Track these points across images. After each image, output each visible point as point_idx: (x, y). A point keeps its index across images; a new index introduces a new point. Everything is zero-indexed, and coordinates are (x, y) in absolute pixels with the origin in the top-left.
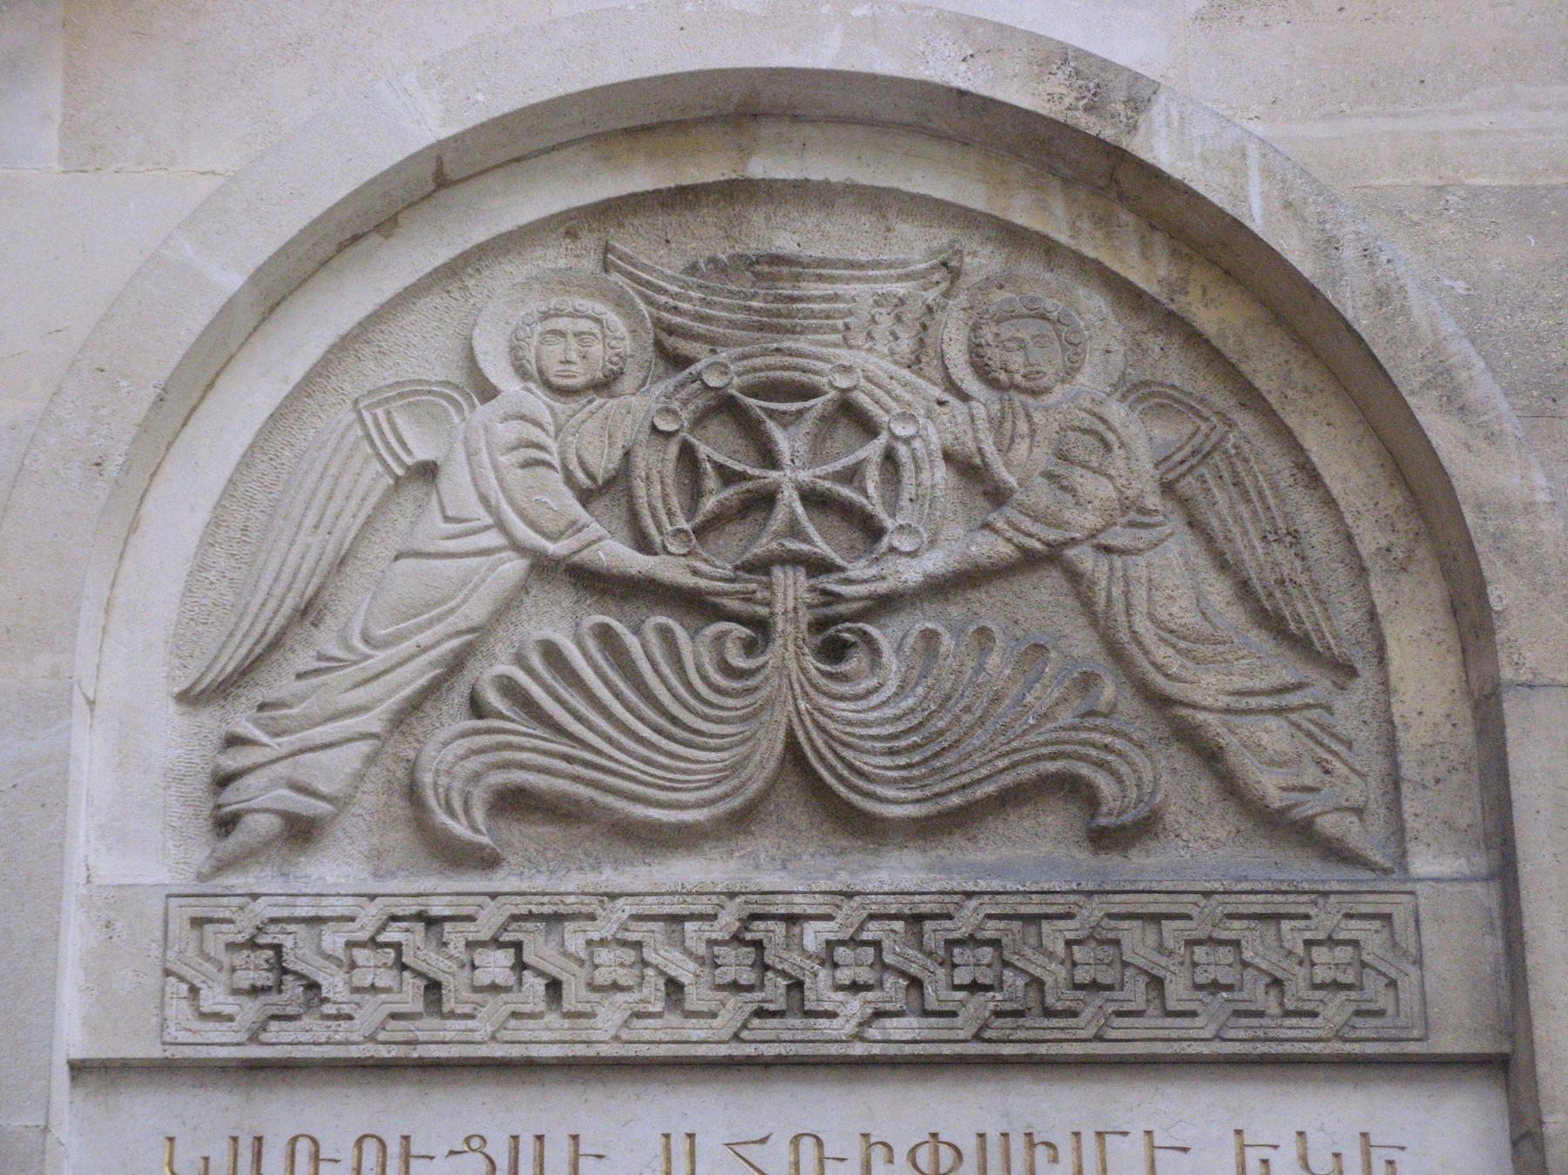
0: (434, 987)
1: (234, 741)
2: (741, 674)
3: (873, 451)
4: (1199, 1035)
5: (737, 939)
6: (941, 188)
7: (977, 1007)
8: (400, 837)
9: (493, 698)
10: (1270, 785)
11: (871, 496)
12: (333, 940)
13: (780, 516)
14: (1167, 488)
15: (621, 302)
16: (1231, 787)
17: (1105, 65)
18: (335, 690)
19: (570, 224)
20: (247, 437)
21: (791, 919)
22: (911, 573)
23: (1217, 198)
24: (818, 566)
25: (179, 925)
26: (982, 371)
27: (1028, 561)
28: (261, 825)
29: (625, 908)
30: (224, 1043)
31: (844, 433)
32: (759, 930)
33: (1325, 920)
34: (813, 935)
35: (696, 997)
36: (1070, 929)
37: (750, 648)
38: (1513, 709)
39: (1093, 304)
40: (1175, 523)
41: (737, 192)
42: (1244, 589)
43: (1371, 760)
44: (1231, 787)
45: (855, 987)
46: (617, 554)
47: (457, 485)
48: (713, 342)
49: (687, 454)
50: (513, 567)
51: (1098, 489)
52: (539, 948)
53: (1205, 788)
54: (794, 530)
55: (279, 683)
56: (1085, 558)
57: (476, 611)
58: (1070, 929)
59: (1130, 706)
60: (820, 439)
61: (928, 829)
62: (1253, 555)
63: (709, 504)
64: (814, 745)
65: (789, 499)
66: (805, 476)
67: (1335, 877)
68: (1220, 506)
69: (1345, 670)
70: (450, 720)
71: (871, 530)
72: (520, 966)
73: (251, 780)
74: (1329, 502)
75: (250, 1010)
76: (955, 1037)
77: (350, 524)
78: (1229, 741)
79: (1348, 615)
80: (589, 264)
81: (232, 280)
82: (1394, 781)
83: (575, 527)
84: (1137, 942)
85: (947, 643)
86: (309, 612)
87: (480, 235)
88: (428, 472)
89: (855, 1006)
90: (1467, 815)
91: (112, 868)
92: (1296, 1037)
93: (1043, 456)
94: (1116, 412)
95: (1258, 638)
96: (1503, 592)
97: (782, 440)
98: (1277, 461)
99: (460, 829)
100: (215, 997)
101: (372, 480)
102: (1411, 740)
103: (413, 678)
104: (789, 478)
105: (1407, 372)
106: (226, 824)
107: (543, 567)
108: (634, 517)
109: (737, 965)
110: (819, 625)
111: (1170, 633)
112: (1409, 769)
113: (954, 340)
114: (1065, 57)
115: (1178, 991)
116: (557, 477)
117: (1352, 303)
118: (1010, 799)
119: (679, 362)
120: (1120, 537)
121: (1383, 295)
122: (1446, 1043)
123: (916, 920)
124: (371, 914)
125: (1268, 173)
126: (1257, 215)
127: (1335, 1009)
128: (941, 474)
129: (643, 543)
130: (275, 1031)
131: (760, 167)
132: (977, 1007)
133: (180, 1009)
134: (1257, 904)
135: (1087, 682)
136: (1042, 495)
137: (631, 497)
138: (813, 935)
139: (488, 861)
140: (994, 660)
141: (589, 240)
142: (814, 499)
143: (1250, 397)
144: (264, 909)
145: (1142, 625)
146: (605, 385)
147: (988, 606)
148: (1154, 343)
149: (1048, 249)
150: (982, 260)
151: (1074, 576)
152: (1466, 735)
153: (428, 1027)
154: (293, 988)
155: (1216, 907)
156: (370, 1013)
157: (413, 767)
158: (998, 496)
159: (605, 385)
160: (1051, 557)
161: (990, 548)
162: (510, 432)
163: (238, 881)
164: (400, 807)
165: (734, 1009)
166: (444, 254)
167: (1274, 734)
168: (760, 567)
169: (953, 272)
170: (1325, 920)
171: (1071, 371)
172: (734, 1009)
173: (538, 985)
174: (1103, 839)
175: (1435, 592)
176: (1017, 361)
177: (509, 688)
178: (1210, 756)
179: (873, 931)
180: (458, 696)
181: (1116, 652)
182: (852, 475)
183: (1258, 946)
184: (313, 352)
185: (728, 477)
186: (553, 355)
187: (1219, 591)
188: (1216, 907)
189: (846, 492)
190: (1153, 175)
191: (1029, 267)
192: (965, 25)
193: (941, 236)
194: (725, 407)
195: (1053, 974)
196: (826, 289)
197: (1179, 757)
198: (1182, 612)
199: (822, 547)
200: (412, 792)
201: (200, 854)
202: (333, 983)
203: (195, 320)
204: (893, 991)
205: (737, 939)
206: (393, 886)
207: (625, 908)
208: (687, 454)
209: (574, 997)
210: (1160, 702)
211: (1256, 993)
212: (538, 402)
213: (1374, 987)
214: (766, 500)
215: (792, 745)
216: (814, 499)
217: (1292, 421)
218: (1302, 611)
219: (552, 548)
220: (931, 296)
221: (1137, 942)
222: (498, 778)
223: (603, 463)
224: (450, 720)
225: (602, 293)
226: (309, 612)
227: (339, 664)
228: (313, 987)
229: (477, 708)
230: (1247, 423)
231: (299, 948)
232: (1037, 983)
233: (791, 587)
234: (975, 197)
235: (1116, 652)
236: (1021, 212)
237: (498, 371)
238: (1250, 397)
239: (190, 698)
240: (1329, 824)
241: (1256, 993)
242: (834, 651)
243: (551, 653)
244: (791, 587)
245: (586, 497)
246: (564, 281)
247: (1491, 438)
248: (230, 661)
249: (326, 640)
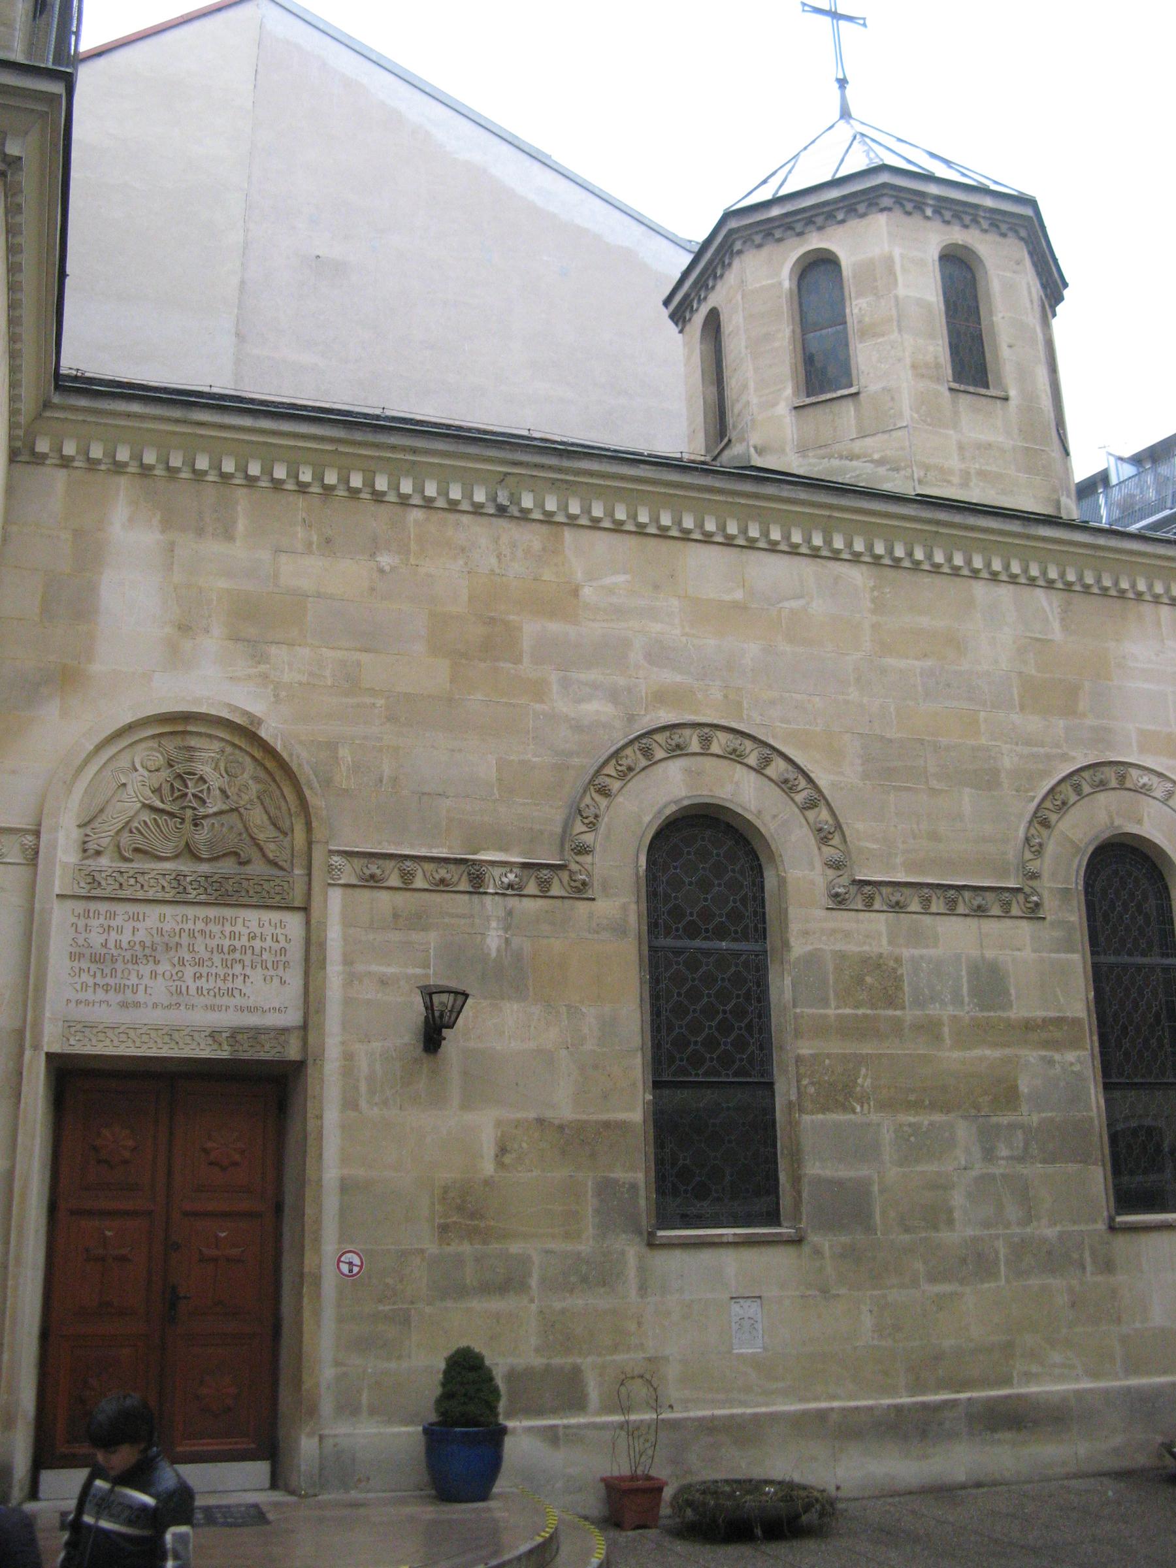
0: (121, 884)
1: (87, 835)
2: (177, 828)
3: (205, 787)
4: (254, 901)
5: (175, 879)
6: (222, 735)
7: (216, 894)
8: (116, 855)
9: (134, 831)
10: (271, 855)
11: (204, 796)
12: (104, 875)
13: (188, 799)
14: (259, 797)
15: (162, 754)
16: (264, 855)
17: (255, 716)
18: (105, 827)
19: (153, 737)
20: (92, 776)
21: (185, 876)
22: (211, 811)
23: (272, 744)
24: (194, 809)
25: (76, 871)
26: (226, 772)
27: (232, 810)
28: (91, 852)
29: (156, 872)
30: (83, 892)
31: (201, 783)
32: (179, 878)
33: (278, 881)
34: (189, 879)
35: (168, 889)
36: (233, 881)
37: (181, 823)
38: (314, 846)
39: (248, 760)
40: (259, 804)
41: (185, 733)
42: (270, 818)
43: (288, 852)
44: (264, 855)
45: (195, 889)
46: (158, 804)
47: (130, 789)
48: (178, 763)
49: (172, 786)
50: (139, 805)
51: (246, 797)
52: (140, 879)
53: (259, 855)
54: (190, 802)
55: (96, 824)
56: (242, 810)
57: (132, 813)
58: (233, 881)
59: (248, 838)
60: (197, 783)
61: (209, 860)
62: (273, 811)
63: (175, 795)
64: (191, 842)
65: (190, 795)
66: (193, 791)
67: (281, 873)
68: (267, 801)
69: (286, 834)
70: (126, 834)
71: (204, 802)
72: (137, 882)
73: (91, 843)
74: (286, 802)
75: (88, 887)
76: (211, 899)
77: (110, 794)
78: (264, 847)
79: (288, 823)
80: (156, 745)
81: (92, 747)
82: (293, 855)
83: (151, 798)
84: (245, 883)
85: (216, 825)
86: (102, 811)
87: (137, 738)
88: (124, 785)
89: (195, 892)
90: (305, 863)
91: (65, 859)
92: (270, 902)
93: (236, 789)
94: (250, 782)
95: (272, 827)
96: (315, 824)
97: (190, 784)
98: (278, 793)
99: (126, 854)
100: (82, 885)
101: (114, 785)
102: (296, 849)
103: (120, 825)
104: (191, 790)
105: (302, 781)
106: (85, 851)
107: (144, 806)
108: (161, 797)
109: (175, 884)
110: (193, 820)
111: (256, 826)
112: (295, 854)
113: (222, 766)
114: (246, 713)
115: (251, 893)
116: (148, 789)
117: (295, 768)
118: (224, 855)
119: (172, 766)
120: (249, 806)
121: (300, 765)
122: (296, 904)
123: (206, 877)
124: (110, 870)
125: (282, 740)
126: (279, 748)
127: (278, 898)
128: (218, 792)
129: (163, 802)
130: (93, 891)
131: (190, 728)
132: (216, 894)
133: (76, 886)
134: (266, 878)
135: (240, 834)
136: (235, 798)
137: (161, 793)
138: (189, 879)
139: (131, 861)
140: (224, 829)
141: (156, 740)
142: (194, 795)
143: (274, 780)
144: (93, 868)
145: (251, 824)
146: (157, 770)
147: (224, 818)
148: (258, 768)
149: (240, 748)
150: (229, 749)
151: (239, 812)
152: (306, 849)
153: (120, 892)
154: (96, 884)
155: (260, 878)
156: (110, 888)
157: (119, 842)
158: (228, 797)
159: (157, 770)
160: (237, 809)
161: (225, 807)
162: (141, 778)
163: (86, 862)
164: (116, 849)
165: (173, 892)
166: (130, 741)
167: (272, 846)
168: (184, 808)
169: (223, 751)
170: (278, 881)
171: (243, 773)
172: (173, 892)
173: (139, 885)
174: (241, 864)
175: (303, 821)
176: (233, 771)
177: (137, 828)
178: (261, 849)
179: (199, 879)
180: (127, 829)
181: (247, 829)
182: (201, 791)
183: (266, 886)
184: (103, 761)
185: (179, 790)
186: (149, 763)
187: (265, 817)
188: (260, 878)
189: (200, 795)
190: (261, 738)
191: (237, 752)
192: (229, 705)
193: (222, 744)
194: (179, 776)
195: (230, 889)
196: (199, 754)
197: (255, 849)
198: (259, 822)
199: (195, 805)
200: (118, 847)
201: (80, 855)
202: (103, 883)
203: (84, 755)
204: (201, 890)
205: (175, 879)
206: (113, 865)
207: (156, 872)
208: (172, 786)
209: (146, 888)
210: (253, 839)
211: (264, 894)
212: (146, 773)
213: (285, 893)
214: (186, 795)
215: (187, 843)
216: (194, 795)
217: (281, 785)
218: (280, 824)
219: (146, 802)
220: (218, 756)
221: (245, 883)
222: (134, 845)
223: (157, 786)
224: (126, 834)
225: (159, 752)
226: (102, 811)
227: (106, 822)
228: (99, 883)
229: (131, 832)
230: (274, 786)
231: (98, 876)
232: (227, 890)
233: (189, 813)
234: (228, 737)
235: (247, 829)
236: (237, 742)
237: (138, 766)
238: (274, 780)
239: (79, 826)
240: (280, 863)
241: (264, 894)
242: (196, 825)
243: (145, 822)
244: (189, 813)
245: (153, 792)
246: (152, 749)
247: (316, 794)
248: (87, 819)
249: (104, 817)
